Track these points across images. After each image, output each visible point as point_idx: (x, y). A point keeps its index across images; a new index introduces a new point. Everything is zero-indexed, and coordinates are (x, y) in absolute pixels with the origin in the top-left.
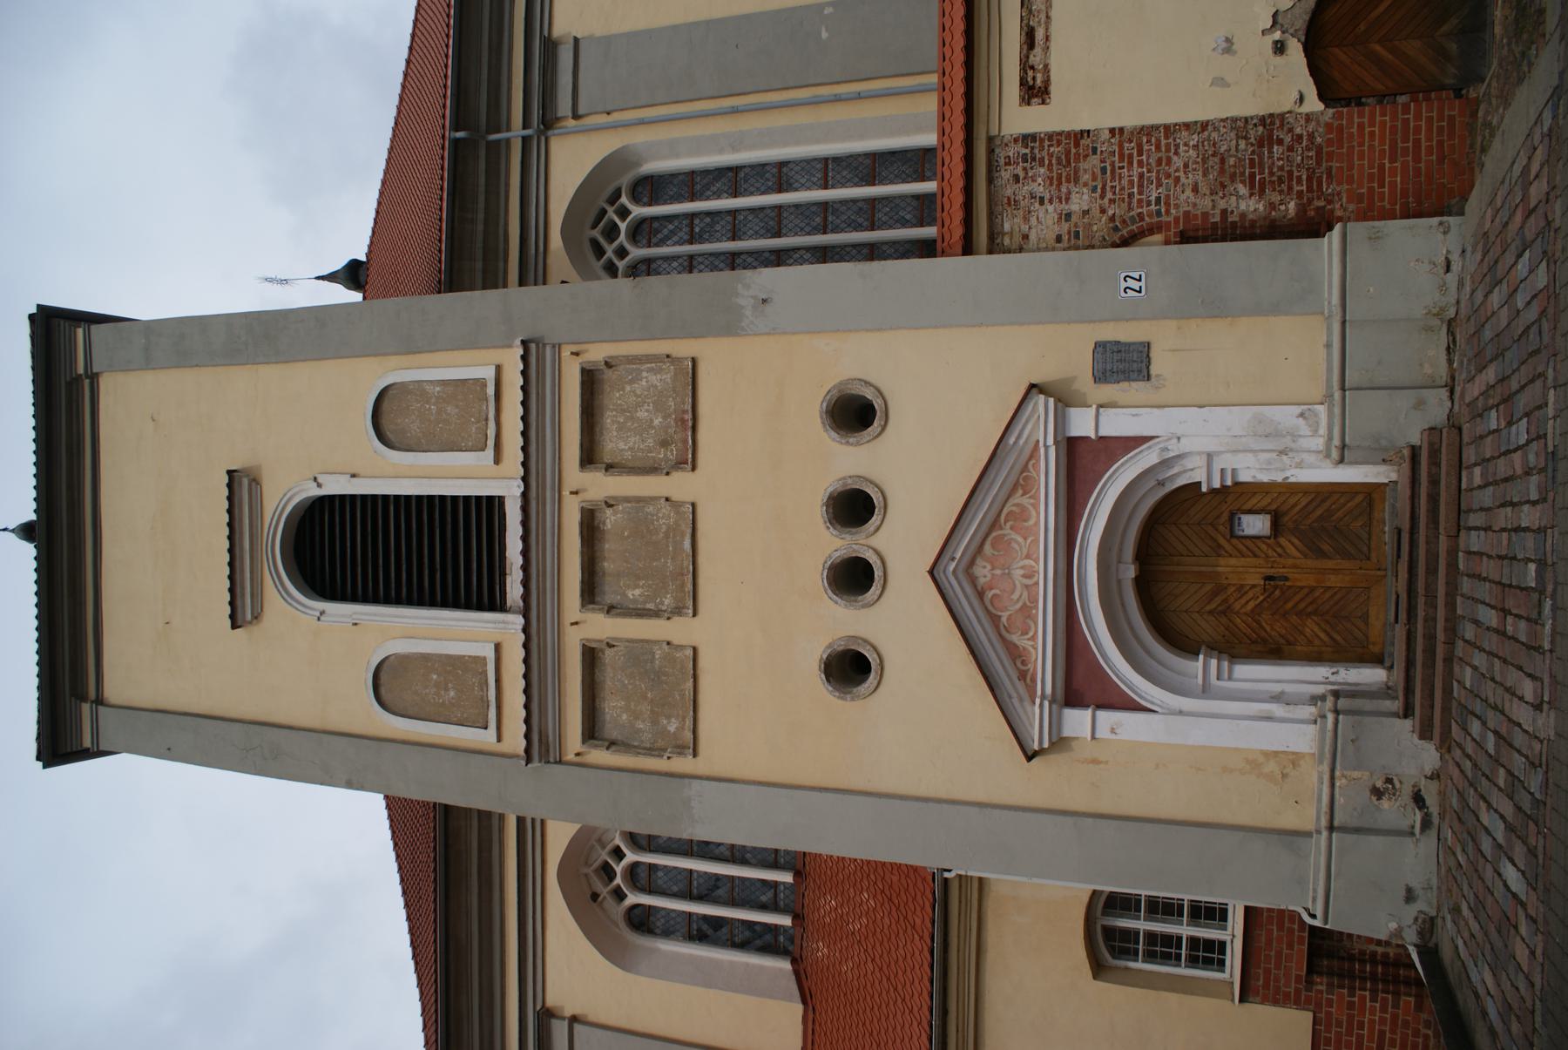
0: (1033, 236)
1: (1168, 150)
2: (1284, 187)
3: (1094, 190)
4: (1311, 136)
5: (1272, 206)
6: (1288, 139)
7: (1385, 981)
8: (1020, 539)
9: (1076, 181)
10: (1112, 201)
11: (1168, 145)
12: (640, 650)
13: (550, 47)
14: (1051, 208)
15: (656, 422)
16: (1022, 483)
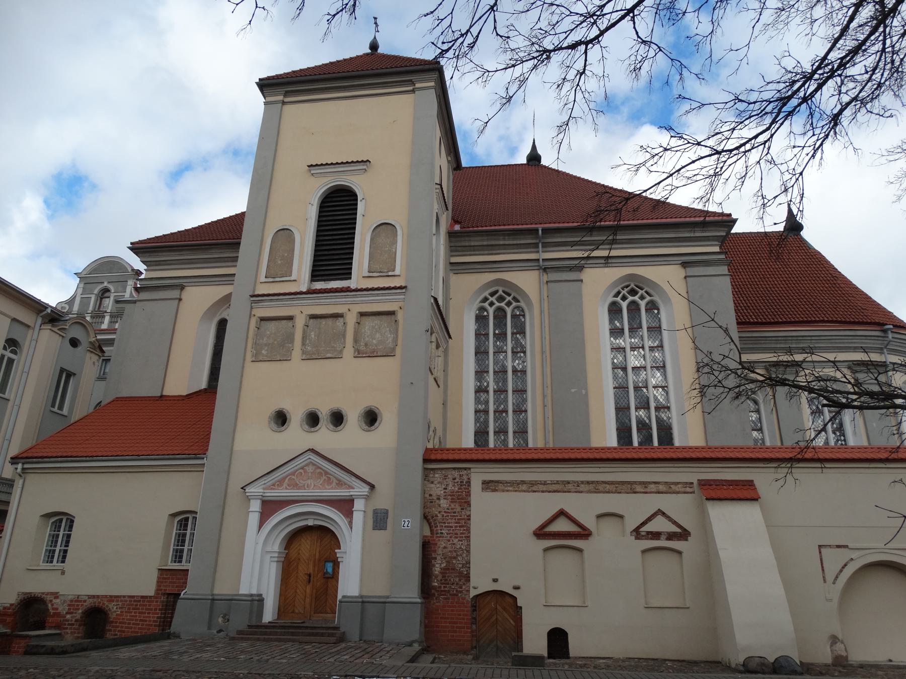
0: (432, 485)
1: (460, 537)
2: (443, 581)
3: (448, 509)
4: (461, 592)
5: (436, 577)
6: (461, 583)
7: (164, 622)
8: (321, 482)
9: (452, 502)
10: (443, 516)
11: (462, 537)
12: (290, 338)
13: (580, 268)
14: (442, 492)
15: (374, 341)
16: (340, 484)
